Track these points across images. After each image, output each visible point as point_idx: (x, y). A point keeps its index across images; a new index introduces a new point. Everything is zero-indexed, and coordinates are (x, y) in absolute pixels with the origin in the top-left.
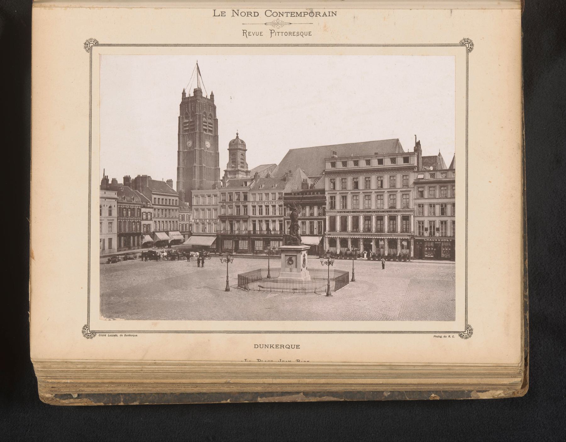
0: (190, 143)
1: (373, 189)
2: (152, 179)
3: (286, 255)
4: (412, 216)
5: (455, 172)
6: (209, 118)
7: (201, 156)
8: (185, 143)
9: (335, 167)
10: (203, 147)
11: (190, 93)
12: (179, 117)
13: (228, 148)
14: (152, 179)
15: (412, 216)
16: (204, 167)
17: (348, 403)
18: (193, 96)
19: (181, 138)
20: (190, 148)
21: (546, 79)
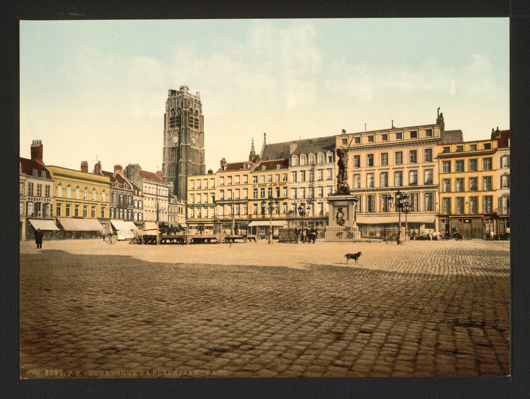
0: (176, 139)
1: (377, 167)
2: (505, 125)
3: (444, 162)
4: (437, 193)
5: (140, 243)
6: (195, 114)
7: (186, 152)
8: (170, 140)
9: (431, 135)
10: (189, 143)
11: (495, 129)
12: (165, 115)
13: (500, 129)
14: (505, 125)
15: (437, 193)
16: (191, 162)
17: (492, 234)
18: (436, 123)
19: (166, 134)
20: (176, 144)
21: (492, 287)
